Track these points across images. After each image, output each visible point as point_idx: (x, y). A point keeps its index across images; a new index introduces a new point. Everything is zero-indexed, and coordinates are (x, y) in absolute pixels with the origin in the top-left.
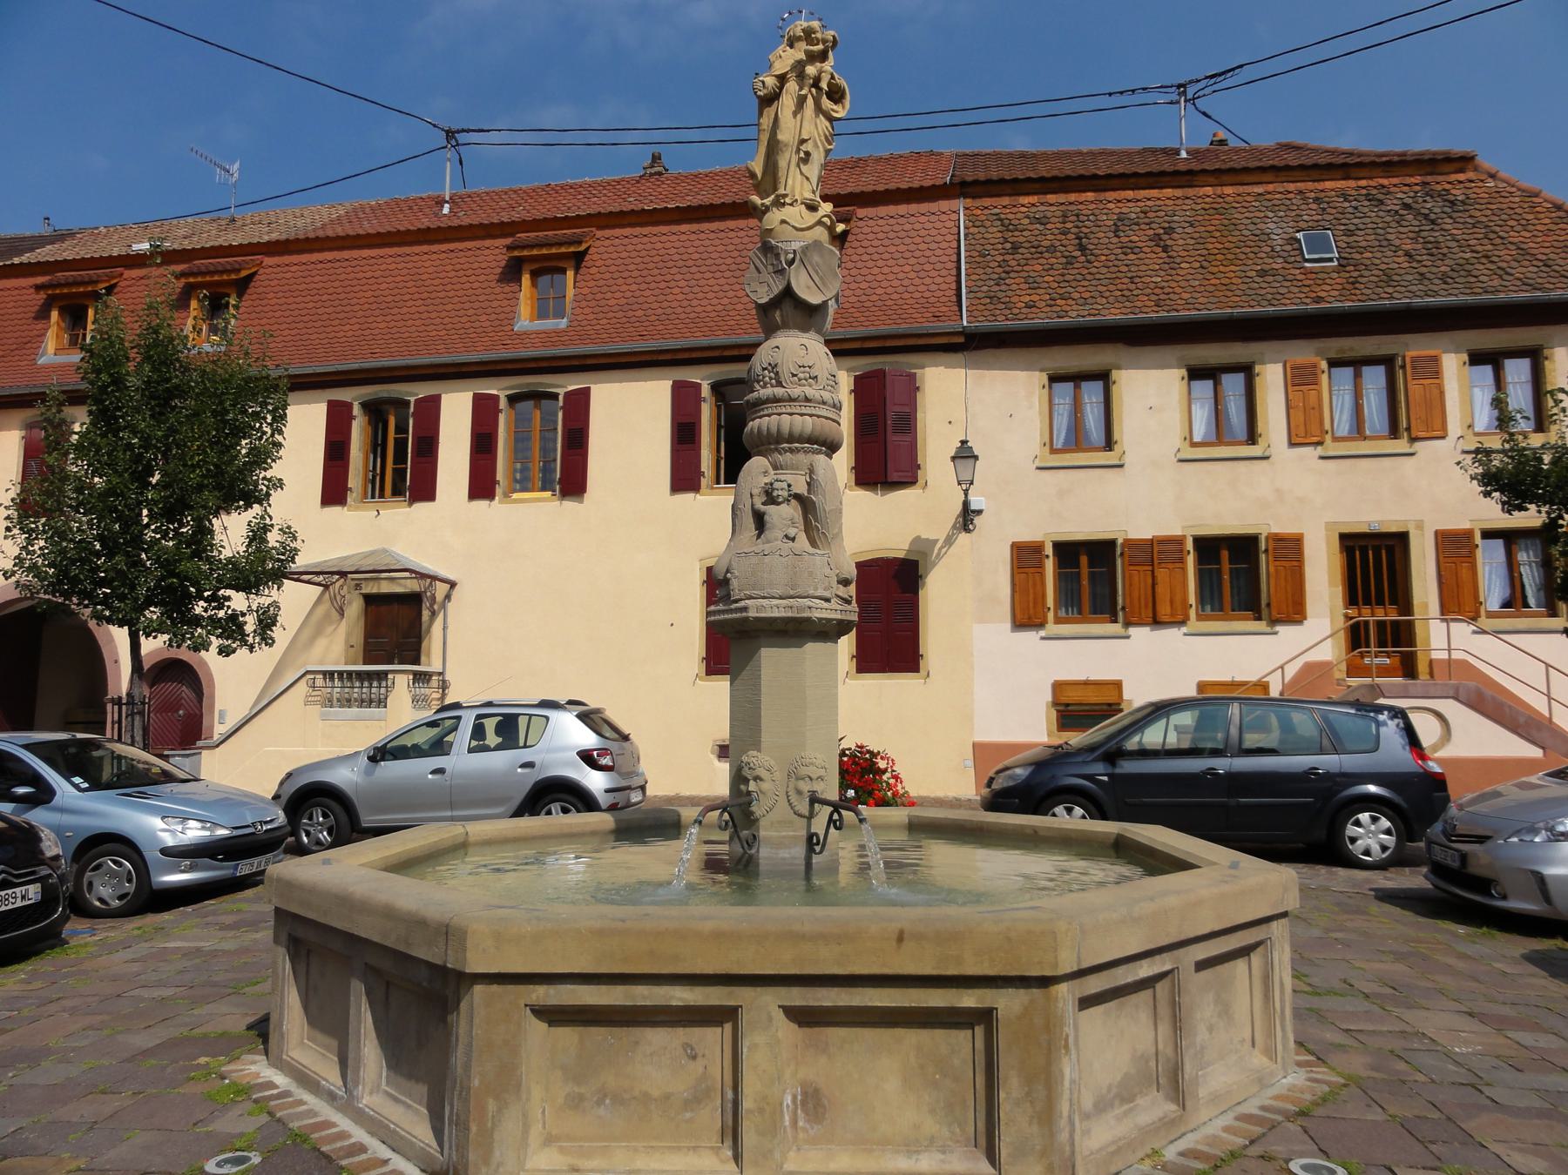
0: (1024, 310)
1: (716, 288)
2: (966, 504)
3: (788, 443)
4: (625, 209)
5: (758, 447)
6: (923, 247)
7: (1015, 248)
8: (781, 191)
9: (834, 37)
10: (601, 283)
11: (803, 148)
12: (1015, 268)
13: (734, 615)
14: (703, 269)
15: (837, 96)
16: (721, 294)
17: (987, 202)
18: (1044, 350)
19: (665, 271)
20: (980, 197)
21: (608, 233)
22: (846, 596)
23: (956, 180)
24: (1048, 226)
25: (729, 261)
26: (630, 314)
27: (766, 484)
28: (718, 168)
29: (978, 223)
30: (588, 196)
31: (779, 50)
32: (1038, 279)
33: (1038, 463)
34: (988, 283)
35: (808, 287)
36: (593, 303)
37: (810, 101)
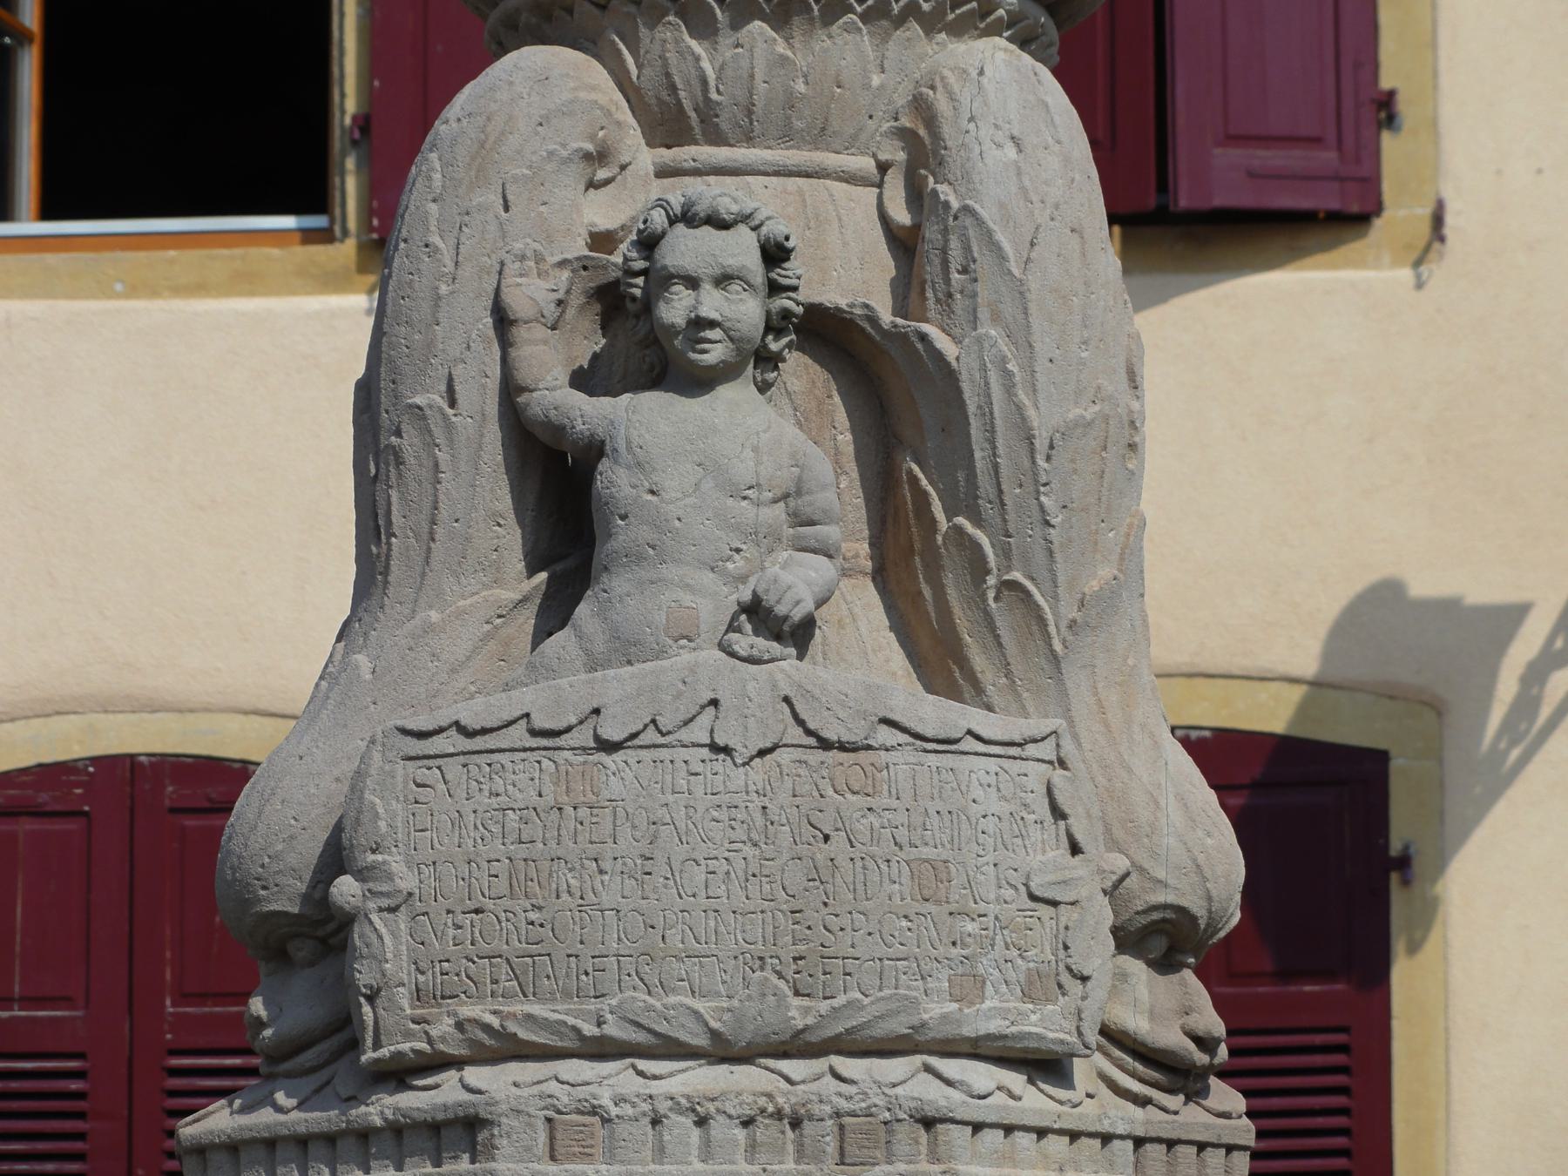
27: (602, 241)
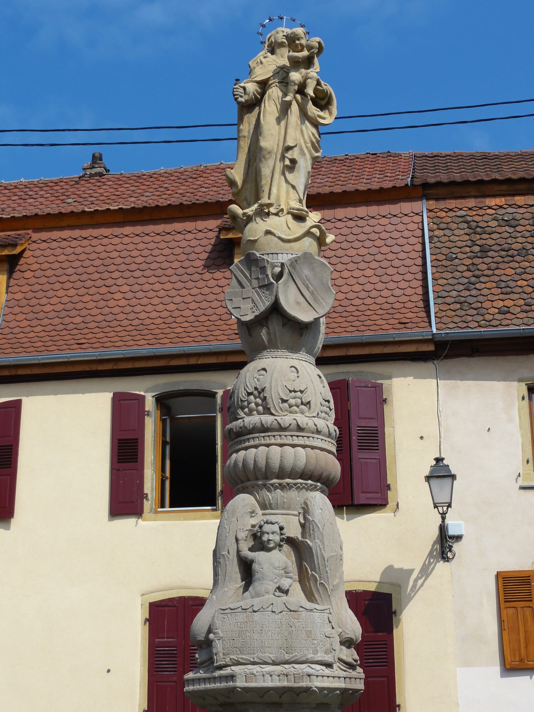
0: (498, 317)
1: (162, 293)
2: (443, 529)
3: (278, 478)
4: (63, 211)
5: (242, 482)
6: (385, 250)
7: (484, 251)
8: (265, 200)
9: (319, 43)
10: (36, 287)
11: (289, 155)
12: (486, 273)
13: (218, 685)
14: (148, 273)
15: (323, 103)
16: (167, 300)
17: (452, 204)
18: (521, 359)
19: (106, 275)
20: (444, 199)
21: (44, 235)
22: (350, 660)
23: (417, 182)
24: (519, 228)
25: (176, 265)
26: (67, 320)
27: (253, 526)
28: (162, 169)
29: (443, 226)
30: (24, 197)
31: (260, 56)
32: (512, 284)
33: (521, 482)
34: (456, 287)
35: (298, 303)
36: (27, 309)
37: (295, 107)
